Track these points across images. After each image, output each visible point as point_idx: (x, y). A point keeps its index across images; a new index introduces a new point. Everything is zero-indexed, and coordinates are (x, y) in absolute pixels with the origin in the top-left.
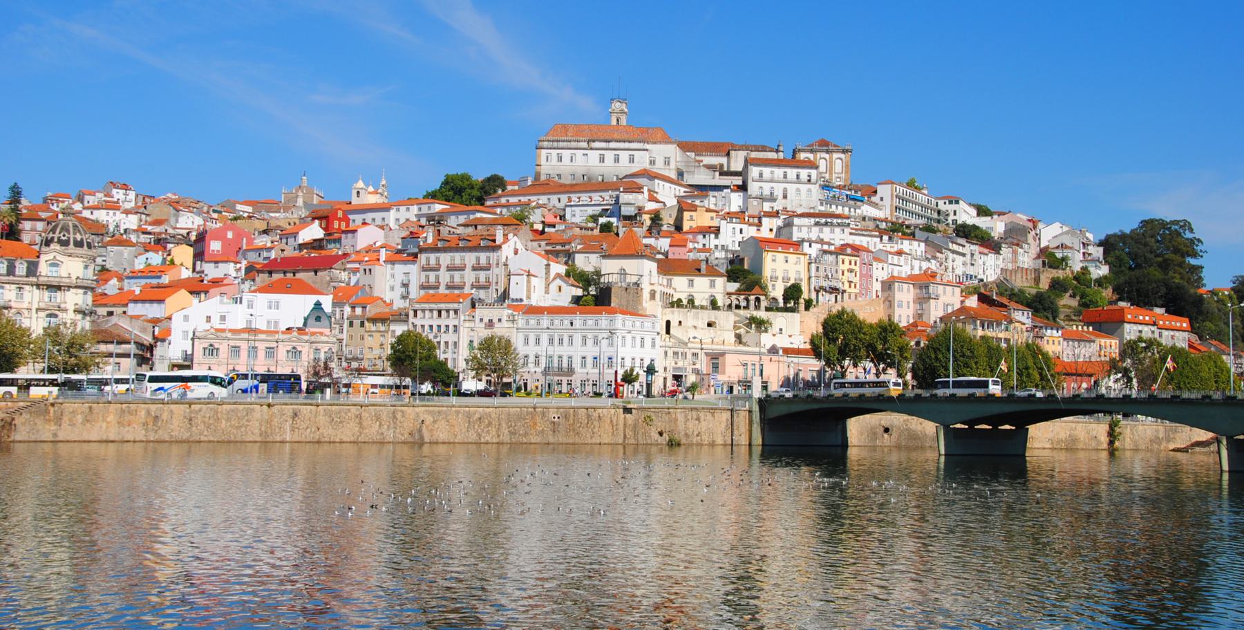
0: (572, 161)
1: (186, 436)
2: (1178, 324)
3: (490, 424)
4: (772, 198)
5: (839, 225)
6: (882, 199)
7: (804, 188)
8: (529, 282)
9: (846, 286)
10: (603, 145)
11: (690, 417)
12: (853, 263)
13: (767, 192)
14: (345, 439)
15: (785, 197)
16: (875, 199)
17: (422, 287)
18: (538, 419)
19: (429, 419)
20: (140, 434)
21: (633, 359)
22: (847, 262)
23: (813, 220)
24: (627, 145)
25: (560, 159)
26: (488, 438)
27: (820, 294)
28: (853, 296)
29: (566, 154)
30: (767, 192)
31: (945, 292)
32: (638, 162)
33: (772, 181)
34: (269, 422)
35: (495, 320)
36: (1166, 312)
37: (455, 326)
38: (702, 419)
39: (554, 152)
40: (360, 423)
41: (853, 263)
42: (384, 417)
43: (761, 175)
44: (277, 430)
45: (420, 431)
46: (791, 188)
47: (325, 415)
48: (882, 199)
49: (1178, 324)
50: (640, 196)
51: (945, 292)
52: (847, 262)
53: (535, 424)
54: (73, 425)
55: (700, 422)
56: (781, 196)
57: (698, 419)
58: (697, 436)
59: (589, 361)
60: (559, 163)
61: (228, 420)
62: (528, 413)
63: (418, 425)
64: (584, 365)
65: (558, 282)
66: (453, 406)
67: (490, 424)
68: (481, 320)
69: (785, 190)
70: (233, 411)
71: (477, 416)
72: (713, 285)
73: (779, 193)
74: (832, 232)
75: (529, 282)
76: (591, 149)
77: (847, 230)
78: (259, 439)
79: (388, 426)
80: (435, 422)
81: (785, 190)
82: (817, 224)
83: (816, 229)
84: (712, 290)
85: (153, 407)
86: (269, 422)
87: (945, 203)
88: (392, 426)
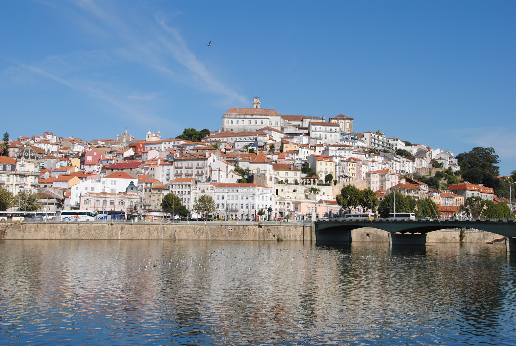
0: (237, 123)
1: (77, 237)
2: (489, 191)
3: (203, 232)
4: (320, 139)
5: (348, 150)
6: (366, 139)
7: (333, 134)
8: (219, 173)
9: (351, 175)
10: (250, 117)
11: (286, 229)
12: (354, 165)
13: (318, 136)
14: (143, 238)
15: (326, 138)
16: (363, 139)
17: (175, 175)
18: (223, 230)
19: (178, 230)
20: (58, 236)
21: (263, 205)
22: (351, 165)
23: (337, 148)
24: (260, 117)
25: (232, 122)
26: (202, 238)
27: (340, 178)
28: (354, 179)
29: (235, 120)
30: (318, 136)
31: (392, 177)
32: (265, 124)
33: (320, 131)
34: (112, 231)
35: (205, 189)
36: (484, 186)
37: (189, 192)
38: (291, 230)
39: (230, 120)
40: (149, 232)
41: (354, 165)
42: (159, 229)
43: (316, 129)
44: (115, 235)
45: (174, 235)
46: (328, 135)
47: (135, 229)
48: (366, 139)
49: (489, 191)
50: (265, 138)
51: (392, 177)
52: (351, 165)
53: (222, 232)
54: (30, 232)
55: (290, 231)
56: (324, 138)
57: (290, 230)
58: (289, 237)
59: (244, 206)
60: (232, 124)
61: (95, 230)
62: (219, 228)
63: (173, 232)
64: (242, 208)
65: (232, 173)
66: (188, 225)
67: (203, 232)
68: (200, 189)
69: (326, 135)
70: (96, 227)
71: (198, 229)
72: (296, 174)
73: (323, 135)
74: (345, 152)
75: (219, 173)
76: (245, 118)
77: (351, 152)
78: (107, 238)
79: (161, 233)
80: (180, 231)
81: (326, 135)
82: (339, 149)
83: (338, 151)
84: (295, 177)
85: (64, 225)
86: (112, 231)
87: (392, 141)
88: (163, 233)
